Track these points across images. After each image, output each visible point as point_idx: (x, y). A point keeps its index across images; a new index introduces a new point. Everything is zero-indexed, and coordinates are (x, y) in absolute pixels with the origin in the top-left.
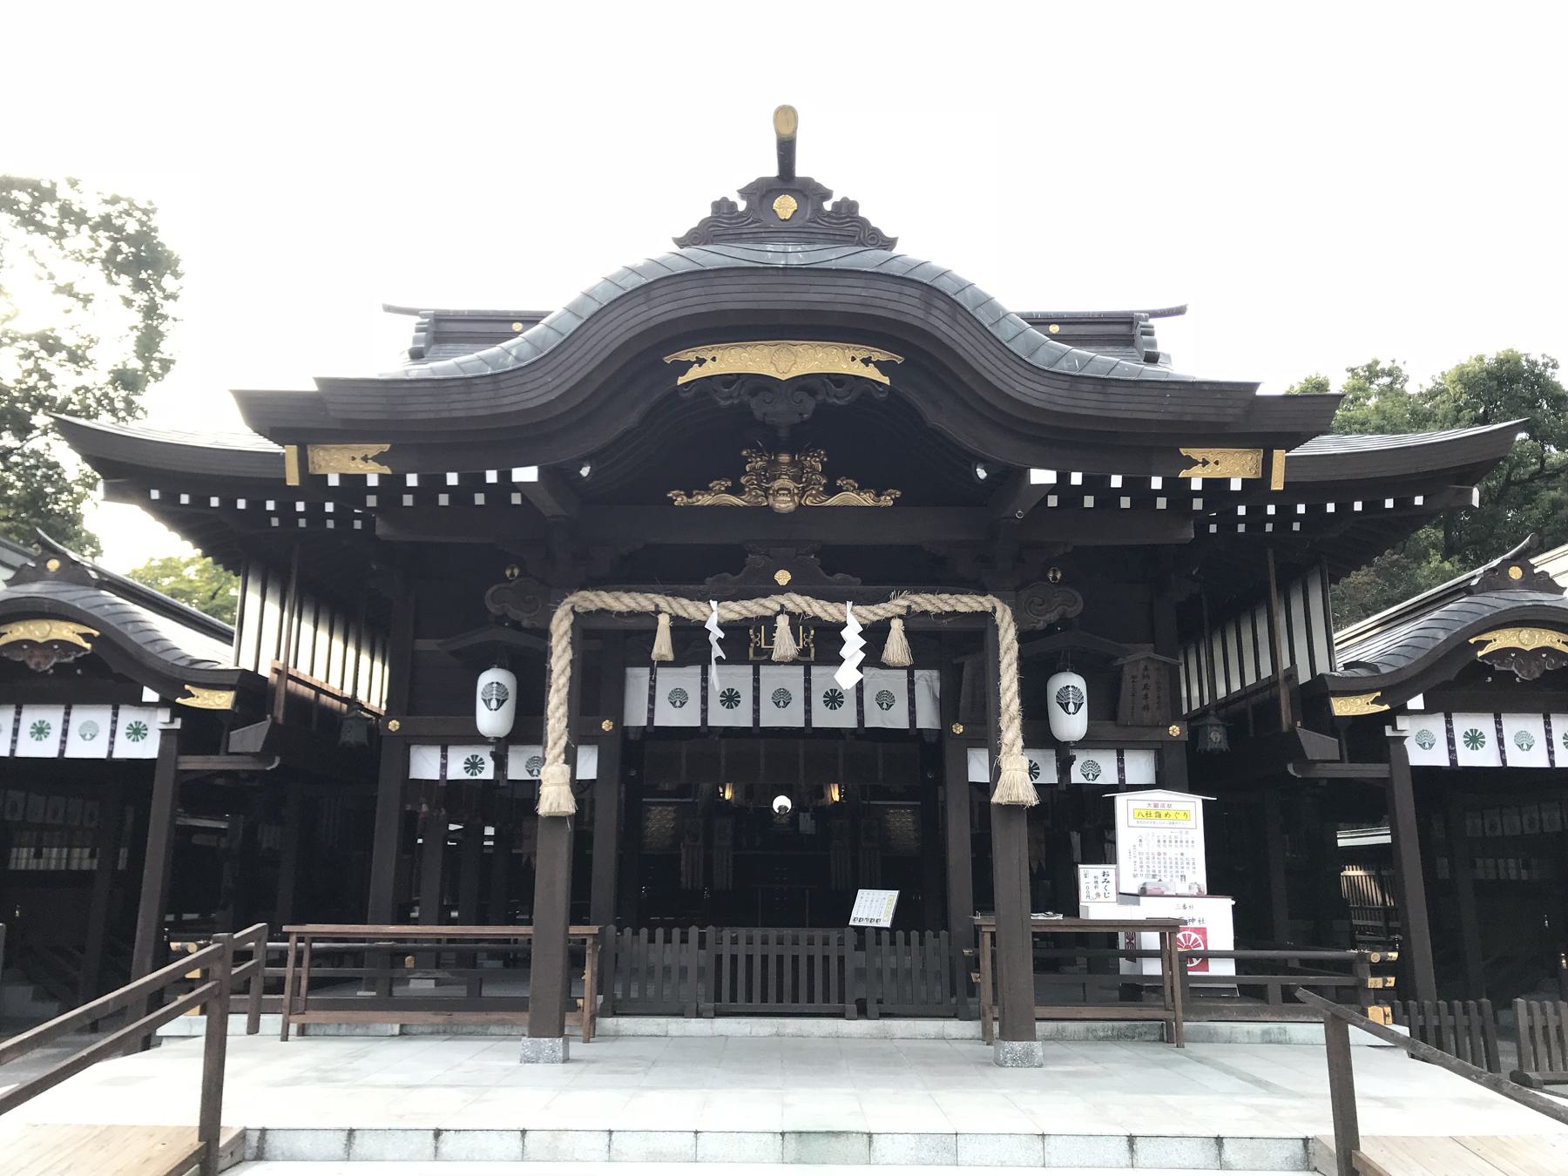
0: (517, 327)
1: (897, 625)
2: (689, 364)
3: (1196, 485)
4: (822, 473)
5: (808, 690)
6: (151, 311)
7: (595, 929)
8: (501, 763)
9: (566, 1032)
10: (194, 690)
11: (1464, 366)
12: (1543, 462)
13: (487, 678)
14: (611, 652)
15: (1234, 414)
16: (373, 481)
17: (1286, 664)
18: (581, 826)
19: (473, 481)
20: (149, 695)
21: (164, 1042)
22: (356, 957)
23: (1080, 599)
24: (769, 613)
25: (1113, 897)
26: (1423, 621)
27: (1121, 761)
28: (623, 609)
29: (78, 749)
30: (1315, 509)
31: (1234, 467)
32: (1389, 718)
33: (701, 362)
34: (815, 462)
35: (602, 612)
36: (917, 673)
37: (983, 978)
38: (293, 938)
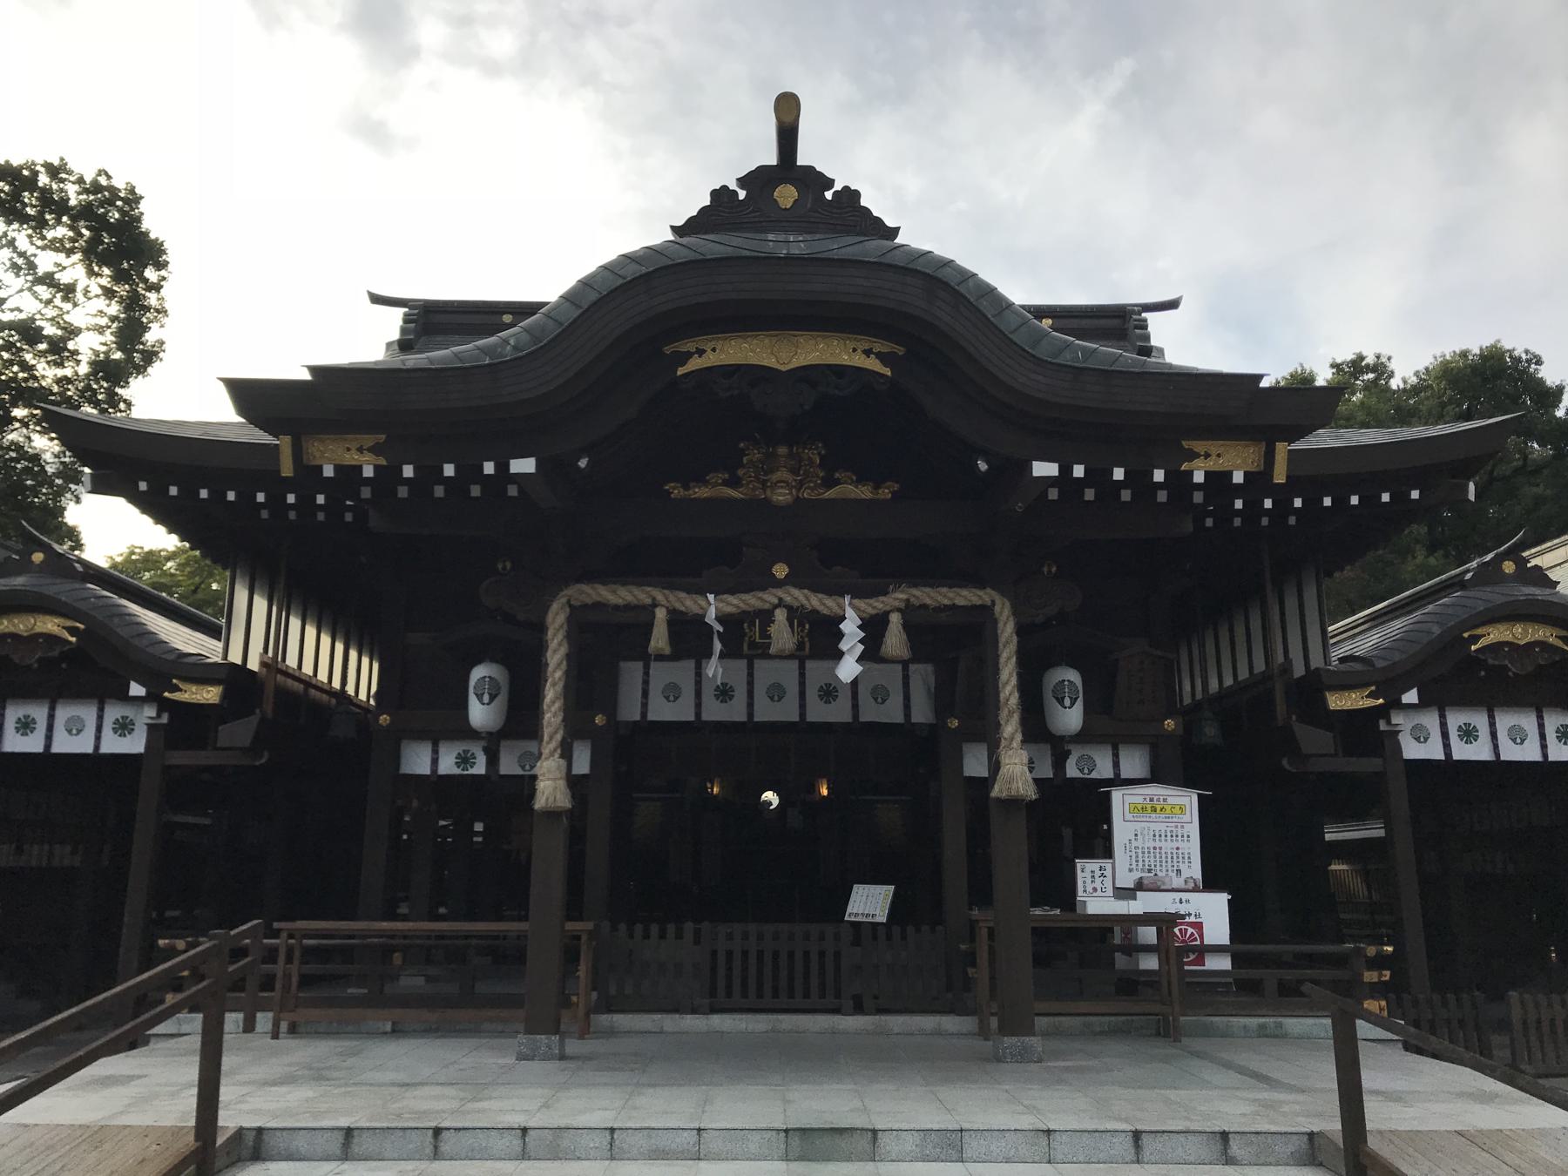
0: (507, 318)
1: (895, 618)
2: (689, 355)
3: (1199, 477)
5: (802, 684)
6: (134, 304)
7: (590, 925)
8: (493, 761)
9: (563, 1027)
11: (1448, 362)
12: (1525, 458)
13: (478, 673)
14: (607, 645)
15: (1231, 403)
16: (368, 472)
17: (1280, 659)
18: (575, 820)
19: (469, 471)
20: (136, 690)
21: (153, 1040)
22: (346, 954)
24: (767, 606)
25: (1110, 892)
26: (1417, 615)
27: (1116, 756)
28: (620, 602)
29: (64, 744)
30: (1312, 502)
31: (1238, 464)
32: (1383, 712)
33: (701, 352)
34: (813, 454)
35: (599, 606)
36: (912, 667)
37: (980, 973)
38: (284, 935)
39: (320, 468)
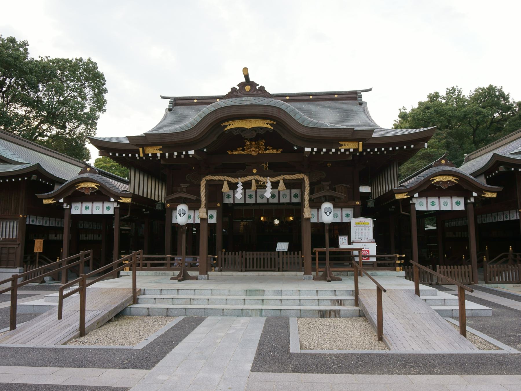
2: (227, 126)
4: (264, 145)
10: (486, 193)
16: (159, 155)
20: (112, 199)
23: (325, 174)
33: (230, 125)
34: (262, 143)
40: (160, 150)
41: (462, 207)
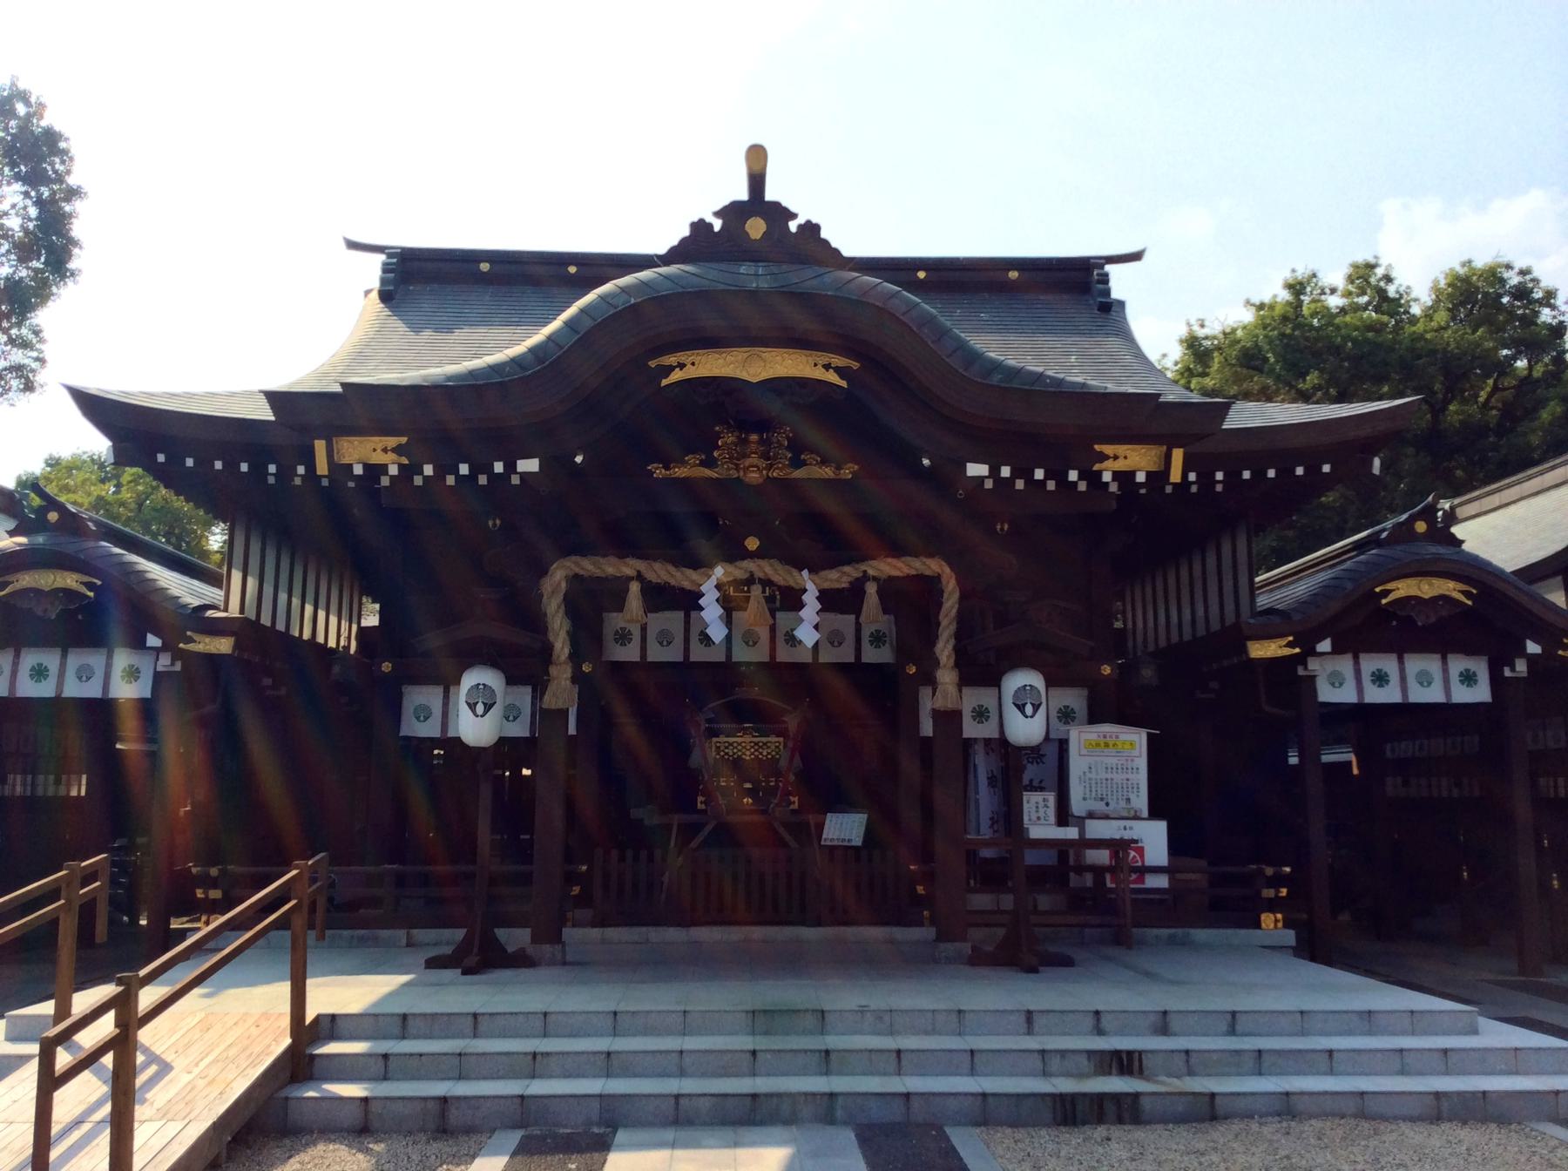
2: (671, 369)
4: (789, 448)
31: (1137, 460)
32: (1301, 660)
33: (682, 366)
39: (350, 466)
40: (398, 450)
41: (1481, 693)
